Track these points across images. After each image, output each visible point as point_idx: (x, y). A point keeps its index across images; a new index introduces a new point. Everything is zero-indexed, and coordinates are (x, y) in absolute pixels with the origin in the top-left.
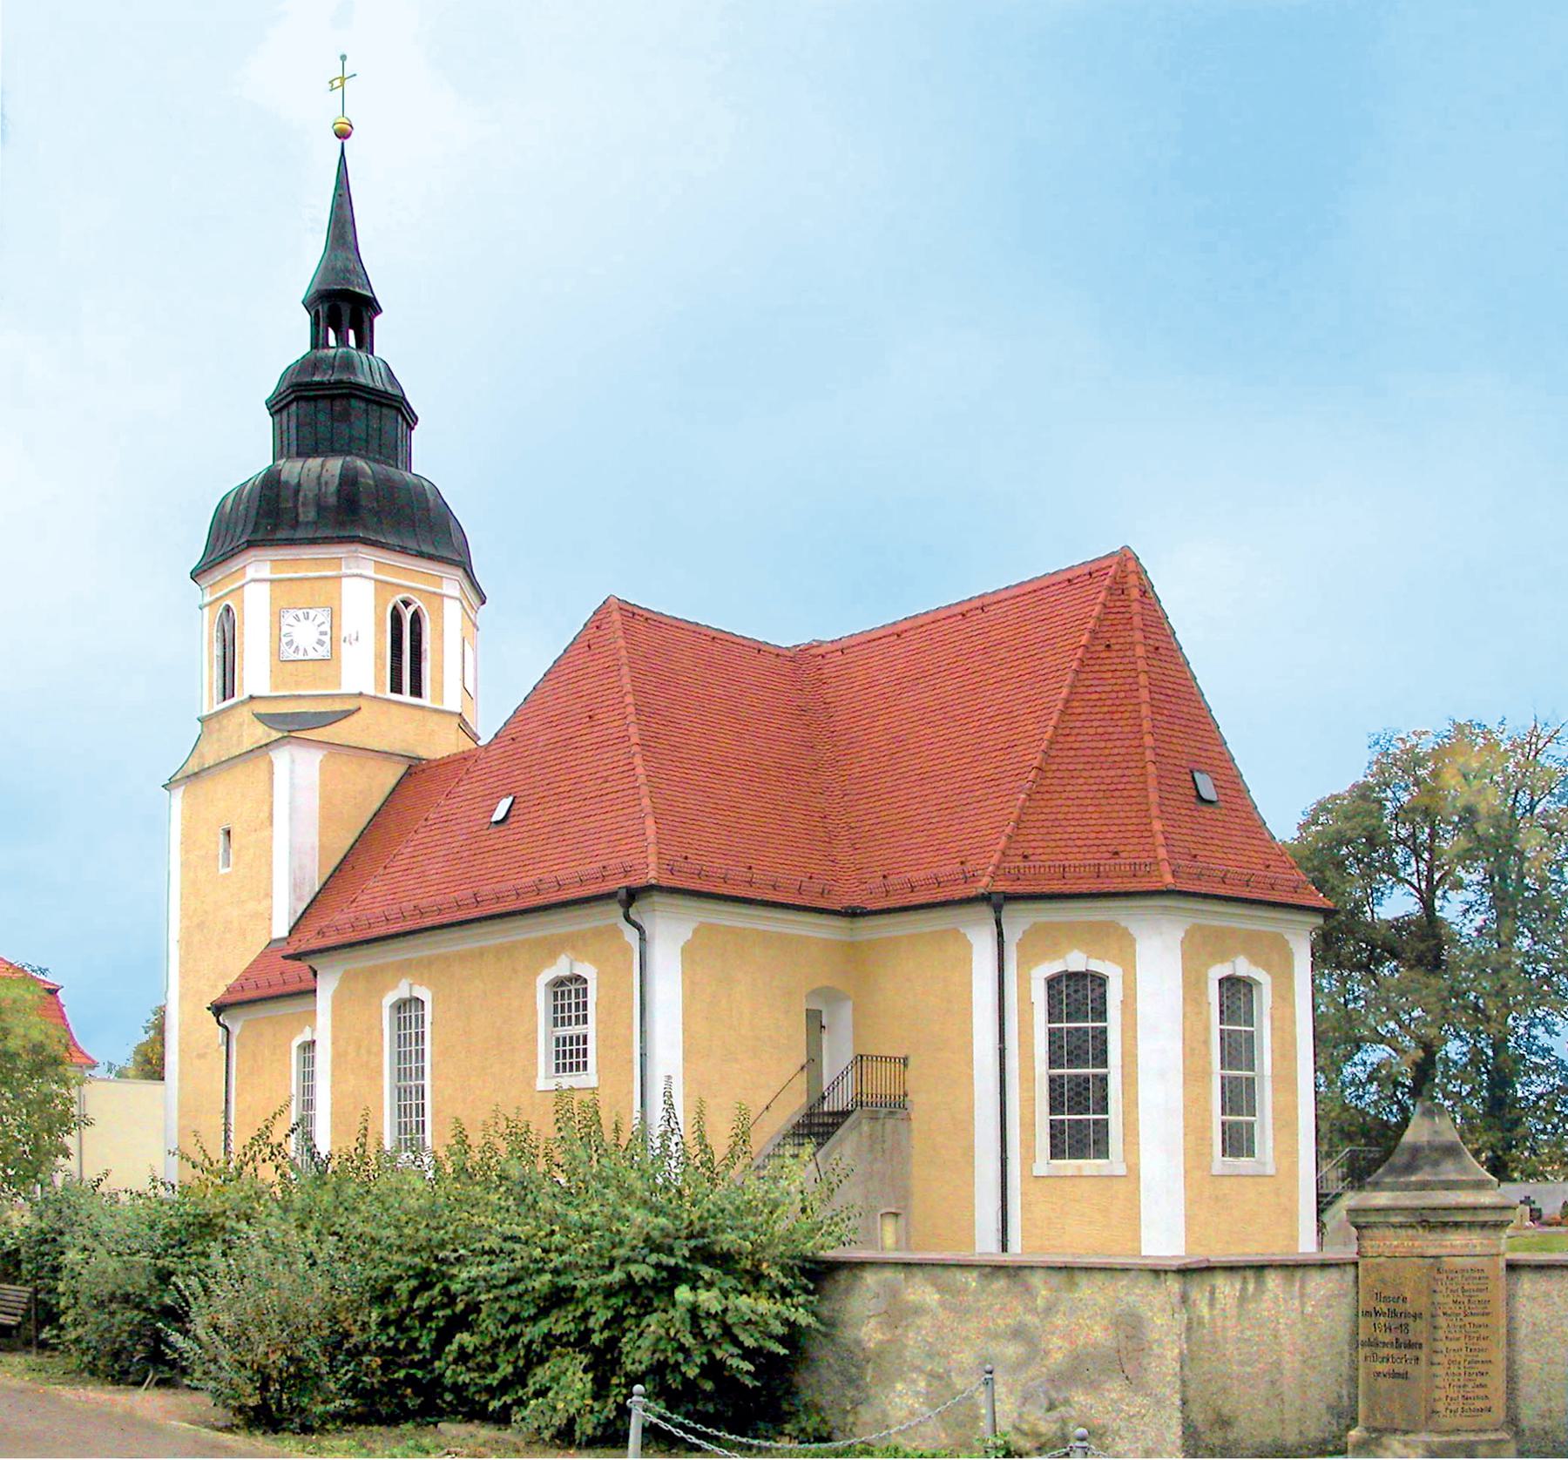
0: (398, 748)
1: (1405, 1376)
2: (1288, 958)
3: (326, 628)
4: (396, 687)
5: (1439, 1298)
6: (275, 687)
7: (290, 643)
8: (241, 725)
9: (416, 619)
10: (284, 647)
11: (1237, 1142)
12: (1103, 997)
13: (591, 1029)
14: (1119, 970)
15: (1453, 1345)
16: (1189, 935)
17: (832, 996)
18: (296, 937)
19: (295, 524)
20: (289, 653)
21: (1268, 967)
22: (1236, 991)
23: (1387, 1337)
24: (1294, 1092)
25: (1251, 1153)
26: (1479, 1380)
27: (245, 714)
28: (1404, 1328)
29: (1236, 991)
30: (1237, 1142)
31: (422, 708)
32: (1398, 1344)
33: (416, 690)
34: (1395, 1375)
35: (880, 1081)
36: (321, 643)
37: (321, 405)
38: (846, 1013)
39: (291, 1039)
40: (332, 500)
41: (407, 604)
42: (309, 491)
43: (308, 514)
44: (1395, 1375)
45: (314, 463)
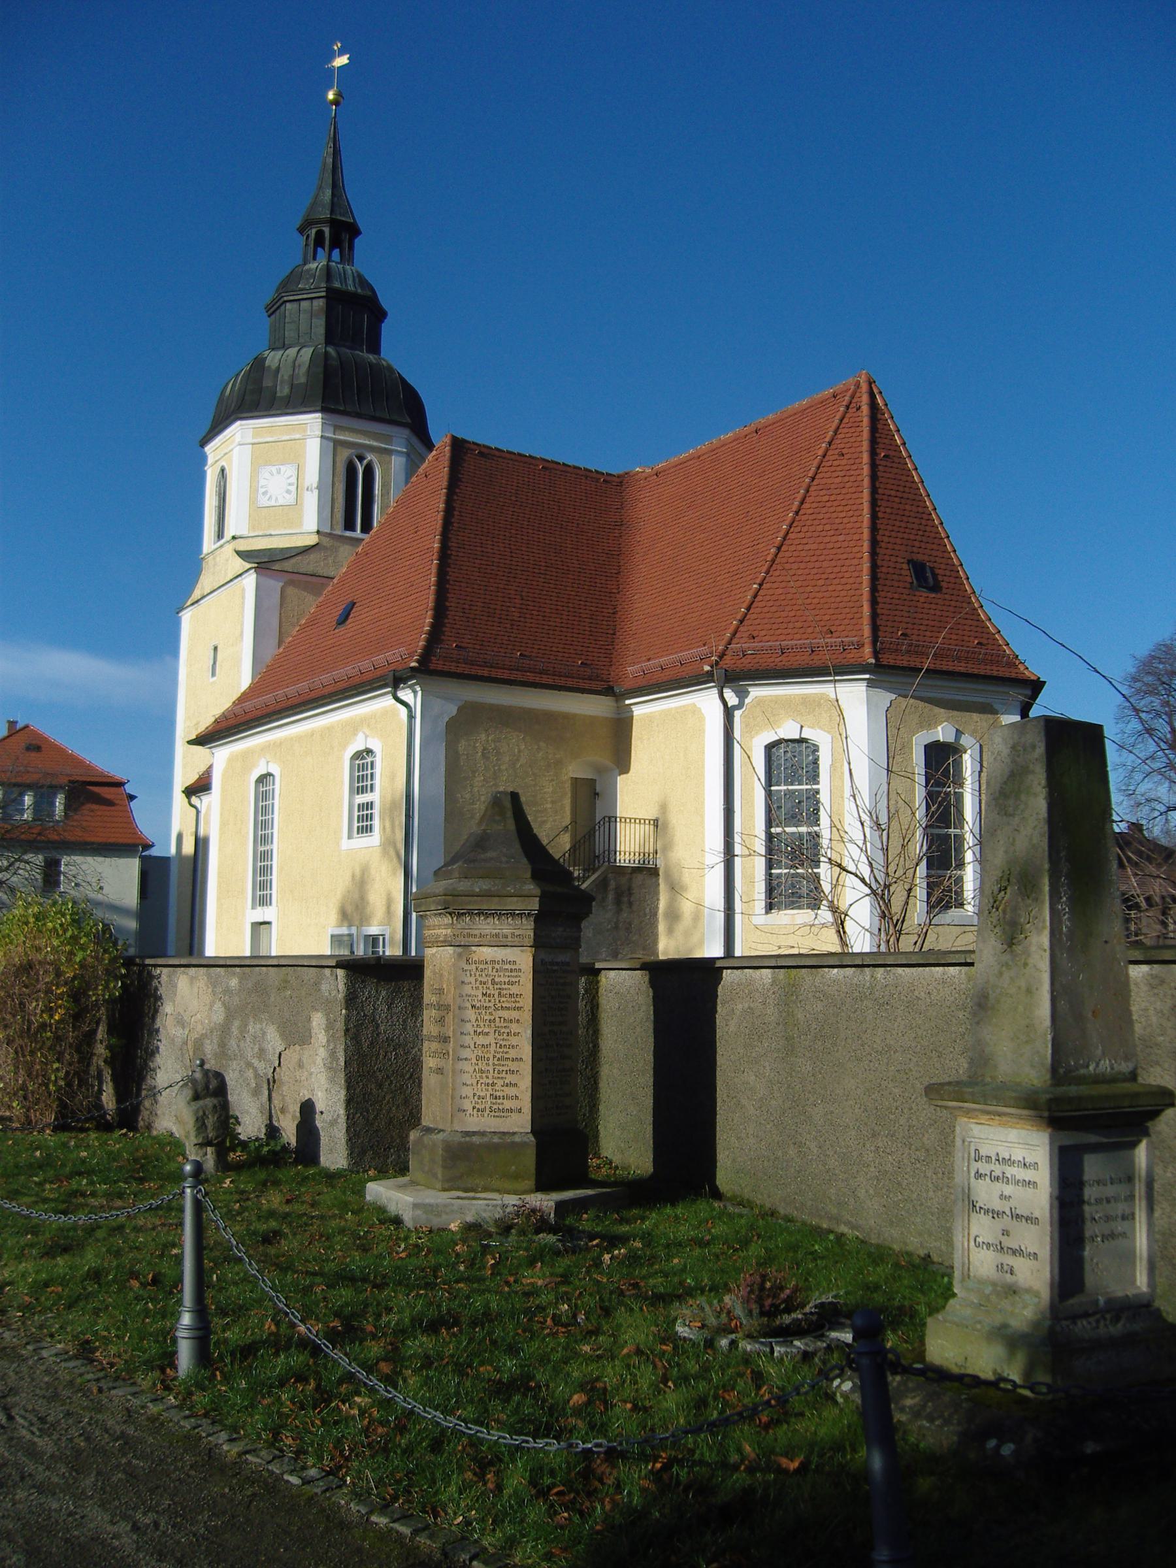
3: (293, 480)
4: (349, 525)
5: (467, 989)
6: (253, 527)
7: (265, 493)
9: (369, 472)
10: (260, 496)
12: (816, 762)
14: (828, 737)
15: (481, 1040)
20: (263, 501)
22: (941, 759)
26: (509, 1078)
27: (229, 549)
29: (941, 759)
36: (288, 492)
40: (303, 380)
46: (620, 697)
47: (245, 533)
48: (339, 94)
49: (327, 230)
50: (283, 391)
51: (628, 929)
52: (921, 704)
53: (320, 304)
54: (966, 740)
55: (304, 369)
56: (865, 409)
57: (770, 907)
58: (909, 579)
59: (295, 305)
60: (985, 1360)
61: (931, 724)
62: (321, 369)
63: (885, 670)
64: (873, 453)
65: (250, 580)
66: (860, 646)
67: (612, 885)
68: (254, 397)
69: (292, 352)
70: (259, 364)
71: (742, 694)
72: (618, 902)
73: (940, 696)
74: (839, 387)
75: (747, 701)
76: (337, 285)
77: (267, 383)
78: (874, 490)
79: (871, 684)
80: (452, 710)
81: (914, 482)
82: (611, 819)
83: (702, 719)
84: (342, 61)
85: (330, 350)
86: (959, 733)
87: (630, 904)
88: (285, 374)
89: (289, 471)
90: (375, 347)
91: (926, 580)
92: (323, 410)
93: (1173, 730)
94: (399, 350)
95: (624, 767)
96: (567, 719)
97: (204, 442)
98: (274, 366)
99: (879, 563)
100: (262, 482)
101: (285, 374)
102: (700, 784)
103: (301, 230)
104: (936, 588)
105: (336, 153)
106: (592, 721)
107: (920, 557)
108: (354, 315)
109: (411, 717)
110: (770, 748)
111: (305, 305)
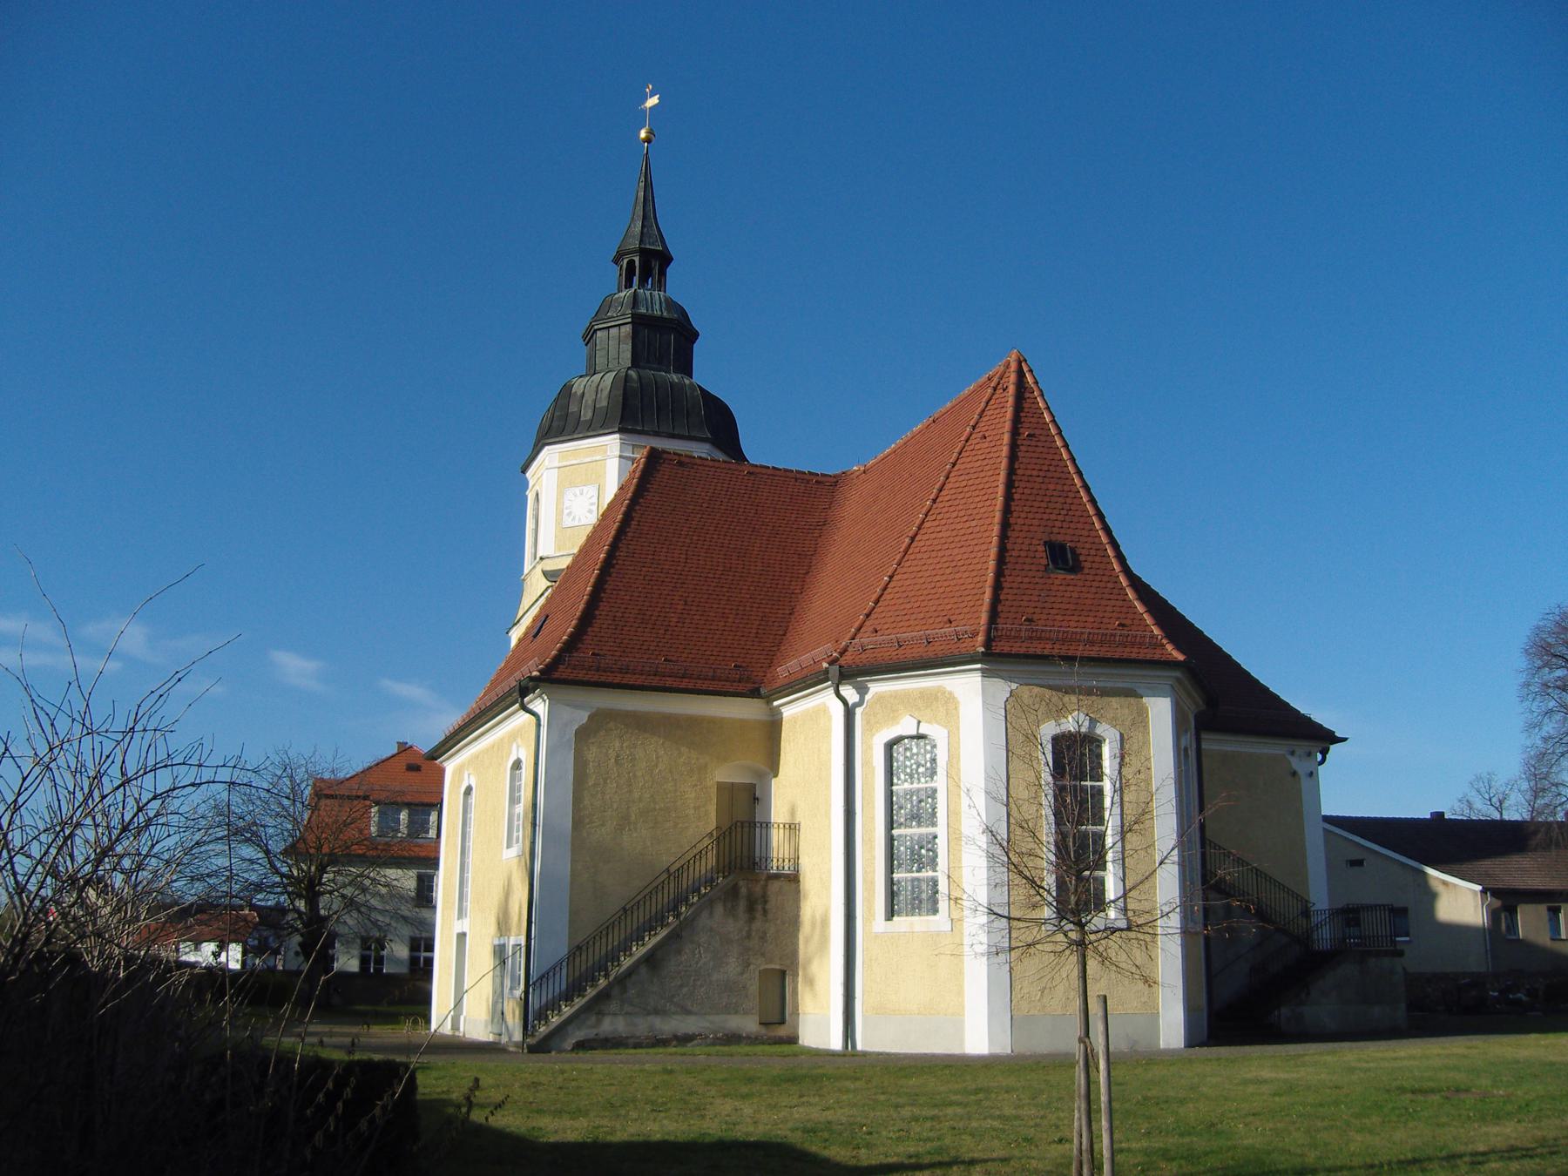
6: (558, 547)
20: (568, 522)
22: (1074, 757)
29: (1074, 757)
36: (590, 511)
40: (604, 403)
46: (769, 699)
47: (551, 553)
48: (650, 132)
49: (637, 259)
50: (587, 415)
51: (763, 938)
52: (1048, 693)
53: (628, 328)
54: (1100, 730)
55: (606, 393)
56: (1012, 389)
57: (891, 913)
58: (1044, 562)
59: (605, 333)
61: (1059, 713)
62: (621, 392)
63: (996, 656)
64: (1015, 432)
66: (974, 635)
67: (744, 891)
68: (562, 424)
69: (597, 377)
70: (566, 391)
71: (862, 691)
72: (751, 909)
73: (1058, 682)
74: (998, 367)
75: (867, 697)
76: (643, 310)
77: (573, 408)
78: (1011, 471)
79: (985, 673)
80: (582, 717)
81: (1061, 460)
82: (767, 825)
83: (830, 719)
84: (653, 101)
85: (632, 373)
86: (1093, 722)
87: (765, 912)
88: (589, 399)
89: (591, 491)
90: (688, 371)
91: (1065, 561)
92: (620, 431)
94: (711, 370)
95: (776, 775)
96: (714, 724)
97: (524, 471)
99: (1009, 546)
100: (567, 504)
101: (589, 399)
102: (828, 787)
103: (616, 261)
104: (1076, 568)
105: (648, 186)
106: (743, 724)
107: (1060, 538)
108: (665, 338)
109: (538, 725)
110: (890, 746)
111: (614, 331)
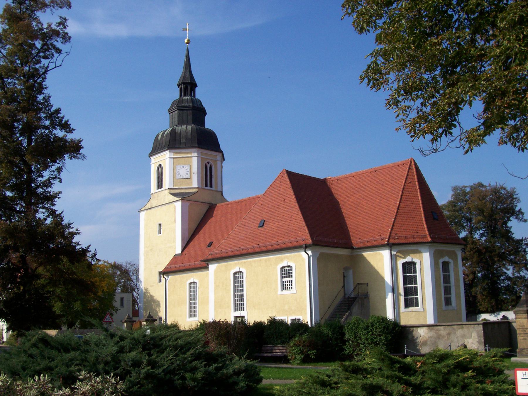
0: (207, 201)
1: (525, 339)
2: (456, 256)
4: (206, 185)
7: (179, 174)
8: (165, 196)
11: (448, 302)
12: (416, 267)
13: (293, 279)
16: (435, 252)
17: (346, 269)
18: (184, 253)
19: (180, 143)
20: (178, 177)
21: (452, 259)
22: (445, 265)
23: (522, 333)
24: (460, 289)
25: (451, 305)
28: (525, 331)
29: (445, 265)
30: (448, 302)
31: (213, 190)
32: (524, 334)
33: (211, 186)
34: (524, 339)
35: (362, 290)
36: (187, 174)
37: (185, 112)
38: (351, 272)
39: (187, 280)
40: (190, 137)
41: (208, 163)
42: (183, 134)
43: (183, 141)
44: (524, 339)
45: (184, 127)
56: (414, 170)
60: (509, 224)
65: (179, 205)
76: (195, 105)
89: (188, 167)
93: (395, 1)
94: (211, 123)
98: (179, 132)
100: (178, 170)
